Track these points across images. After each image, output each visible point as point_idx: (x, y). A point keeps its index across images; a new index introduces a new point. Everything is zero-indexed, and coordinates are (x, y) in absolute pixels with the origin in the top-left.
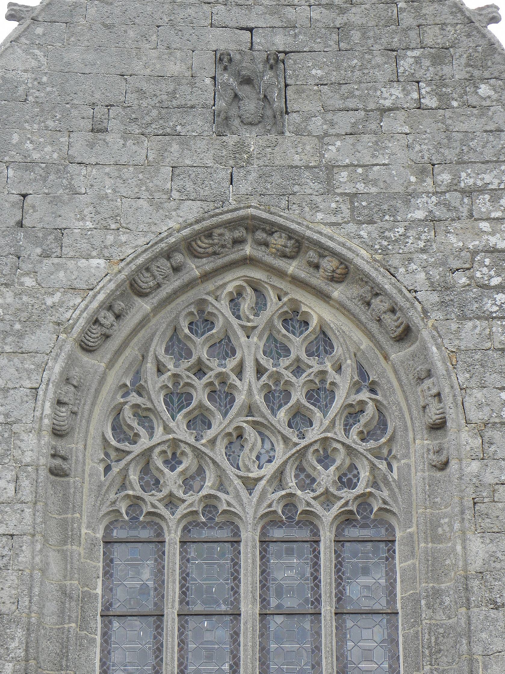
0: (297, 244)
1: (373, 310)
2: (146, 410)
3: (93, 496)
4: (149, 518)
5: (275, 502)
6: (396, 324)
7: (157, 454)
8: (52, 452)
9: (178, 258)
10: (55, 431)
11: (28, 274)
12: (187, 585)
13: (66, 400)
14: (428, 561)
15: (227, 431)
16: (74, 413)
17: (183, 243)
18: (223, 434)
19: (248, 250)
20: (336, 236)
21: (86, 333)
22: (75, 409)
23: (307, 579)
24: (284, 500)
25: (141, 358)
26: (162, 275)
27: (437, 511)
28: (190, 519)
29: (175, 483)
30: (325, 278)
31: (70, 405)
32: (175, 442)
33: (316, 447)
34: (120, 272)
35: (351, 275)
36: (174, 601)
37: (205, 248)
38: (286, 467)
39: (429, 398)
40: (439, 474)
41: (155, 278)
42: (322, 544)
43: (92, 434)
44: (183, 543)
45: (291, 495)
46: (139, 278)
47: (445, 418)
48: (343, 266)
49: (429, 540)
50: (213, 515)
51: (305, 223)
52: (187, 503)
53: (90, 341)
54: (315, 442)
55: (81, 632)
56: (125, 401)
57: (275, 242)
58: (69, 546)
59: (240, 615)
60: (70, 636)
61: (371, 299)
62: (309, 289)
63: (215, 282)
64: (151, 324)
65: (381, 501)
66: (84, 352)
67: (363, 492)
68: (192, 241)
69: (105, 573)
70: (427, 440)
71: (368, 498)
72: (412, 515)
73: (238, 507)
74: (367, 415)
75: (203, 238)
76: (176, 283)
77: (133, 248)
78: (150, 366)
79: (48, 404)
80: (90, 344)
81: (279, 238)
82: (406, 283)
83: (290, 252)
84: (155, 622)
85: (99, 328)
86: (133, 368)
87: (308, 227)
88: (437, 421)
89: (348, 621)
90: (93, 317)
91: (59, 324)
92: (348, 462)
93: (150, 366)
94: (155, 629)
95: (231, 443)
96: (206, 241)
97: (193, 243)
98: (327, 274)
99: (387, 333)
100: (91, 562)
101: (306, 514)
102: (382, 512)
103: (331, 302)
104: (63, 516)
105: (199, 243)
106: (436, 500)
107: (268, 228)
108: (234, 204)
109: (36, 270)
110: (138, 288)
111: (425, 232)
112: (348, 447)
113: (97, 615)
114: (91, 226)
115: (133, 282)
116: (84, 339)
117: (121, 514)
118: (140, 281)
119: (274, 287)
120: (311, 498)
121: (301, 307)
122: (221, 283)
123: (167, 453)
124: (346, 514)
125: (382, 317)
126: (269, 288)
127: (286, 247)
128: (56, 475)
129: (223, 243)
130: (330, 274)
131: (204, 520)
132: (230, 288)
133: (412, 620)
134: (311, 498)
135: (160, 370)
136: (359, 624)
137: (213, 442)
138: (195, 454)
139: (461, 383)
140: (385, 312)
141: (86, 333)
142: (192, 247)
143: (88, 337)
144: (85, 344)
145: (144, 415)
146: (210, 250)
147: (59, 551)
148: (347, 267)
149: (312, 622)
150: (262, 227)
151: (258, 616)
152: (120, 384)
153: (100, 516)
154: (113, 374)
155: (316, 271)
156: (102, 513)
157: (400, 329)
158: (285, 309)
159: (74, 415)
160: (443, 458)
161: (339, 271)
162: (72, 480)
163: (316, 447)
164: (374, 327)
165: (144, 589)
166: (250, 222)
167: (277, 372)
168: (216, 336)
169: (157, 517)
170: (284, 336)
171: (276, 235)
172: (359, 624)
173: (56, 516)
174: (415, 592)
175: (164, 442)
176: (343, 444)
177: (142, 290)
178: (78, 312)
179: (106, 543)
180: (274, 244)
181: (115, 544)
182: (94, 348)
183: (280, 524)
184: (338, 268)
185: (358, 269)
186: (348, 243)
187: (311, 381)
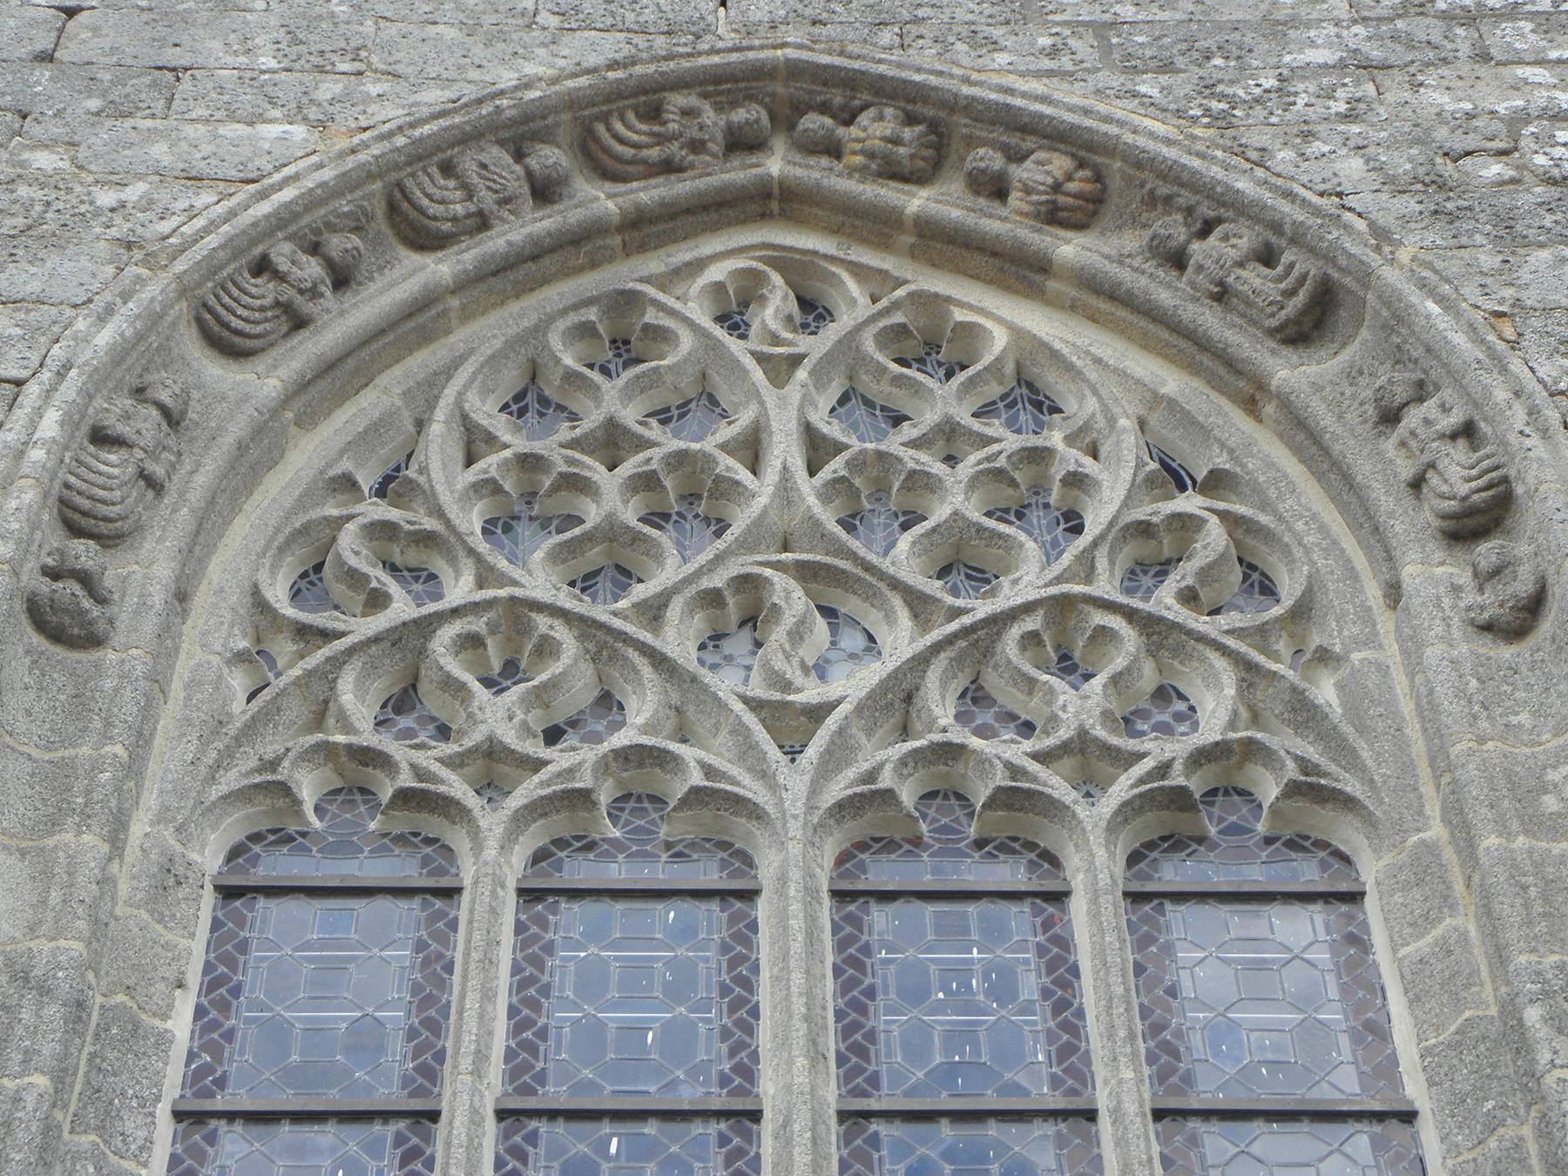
0: (933, 137)
1: (1200, 268)
2: (417, 542)
3: (194, 737)
4: (403, 822)
5: (888, 767)
6: (1282, 286)
7: (447, 641)
8: (50, 561)
9: (550, 157)
10: (70, 514)
11: (47, 146)
12: (541, 1022)
13: (122, 429)
14: (1525, 888)
15: (706, 583)
16: (154, 485)
17: (565, 117)
18: (691, 591)
19: (776, 164)
20: (1056, 95)
21: (224, 288)
22: (159, 471)
23: (1026, 1009)
24: (921, 773)
25: (412, 429)
26: (496, 192)
27: (1528, 750)
28: (559, 824)
29: (511, 718)
30: (1026, 215)
31: (136, 450)
32: (519, 611)
33: (1032, 623)
34: (353, 151)
35: (1115, 200)
36: (481, 1057)
37: (636, 146)
38: (923, 678)
39: (1435, 445)
40: (1506, 652)
41: (469, 192)
42: (1078, 906)
43: (215, 581)
44: (529, 895)
45: (949, 752)
46: (418, 184)
47: (1505, 480)
48: (1087, 173)
49: (1515, 825)
50: (653, 822)
51: (957, 71)
52: (545, 773)
53: (235, 315)
54: (1028, 608)
55: (76, 1138)
56: (345, 512)
57: (862, 135)
58: (68, 837)
59: (755, 1116)
60: (19, 1115)
61: (1189, 242)
62: (977, 259)
63: (669, 256)
64: (452, 339)
65: (1290, 764)
66: (209, 352)
67: (1219, 738)
68: (597, 118)
69: (212, 983)
70: (1442, 564)
71: (1240, 766)
72: (1420, 797)
73: (746, 779)
74: (1205, 547)
75: (630, 115)
76: (539, 224)
77: (403, 107)
78: (440, 438)
79: (50, 425)
80: (236, 323)
81: (874, 120)
82: (1305, 179)
83: (912, 157)
84: (400, 1140)
85: (271, 285)
86: (383, 444)
87: (966, 80)
88: (1475, 497)
89: (1208, 1141)
90: (254, 242)
91: (129, 246)
92: (1149, 677)
93: (440, 438)
94: (397, 1162)
95: (717, 637)
96: (644, 127)
97: (600, 128)
98: (1035, 198)
99: (1254, 323)
100: (159, 928)
101: (1009, 807)
102: (1301, 803)
103: (1052, 285)
104: (59, 754)
105: (619, 127)
106: (1514, 720)
107: (838, 100)
108: (730, 39)
109: (77, 138)
110: (413, 214)
111: (1345, 85)
112: (1149, 625)
113: (158, 1099)
114: (273, 64)
115: (398, 195)
116: (212, 301)
117: (297, 802)
118: (418, 193)
119: (857, 270)
120: (1027, 754)
121: (949, 312)
122: (688, 257)
123: (484, 645)
124: (1161, 807)
125: (1230, 280)
126: (845, 276)
127: (896, 141)
128: (57, 635)
129: (694, 133)
130: (1044, 198)
131: (616, 833)
132: (717, 273)
133: (1490, 1105)
134: (1027, 754)
135: (475, 443)
136: (1256, 1148)
137: (653, 612)
138: (588, 652)
139: (1549, 381)
140: (1240, 264)
141: (224, 288)
142: (597, 140)
143: (226, 300)
144: (217, 318)
145: (413, 563)
146: (654, 153)
147: (23, 853)
148: (1098, 178)
149: (1061, 1142)
150: (819, 99)
151: (833, 1121)
152: (332, 473)
153: (212, 798)
154: (311, 447)
155: (996, 204)
156: (215, 792)
157: (1301, 297)
158: (898, 318)
159: (150, 494)
160: (1523, 585)
161: (1072, 186)
162: (111, 656)
163: (1032, 623)
164: (1210, 320)
165: (365, 1039)
166: (780, 89)
167: (881, 455)
168: (669, 379)
169: (432, 811)
170: (898, 380)
171: (864, 119)
172: (1256, 1148)
173: (35, 753)
174: (1480, 1013)
175: (474, 608)
176: (1130, 614)
177: (426, 221)
178: (199, 223)
179: (228, 893)
180: (858, 140)
181: (261, 902)
182: (250, 343)
183: (907, 847)
184: (1069, 178)
185: (1140, 162)
186: (1102, 108)
187: (998, 474)
